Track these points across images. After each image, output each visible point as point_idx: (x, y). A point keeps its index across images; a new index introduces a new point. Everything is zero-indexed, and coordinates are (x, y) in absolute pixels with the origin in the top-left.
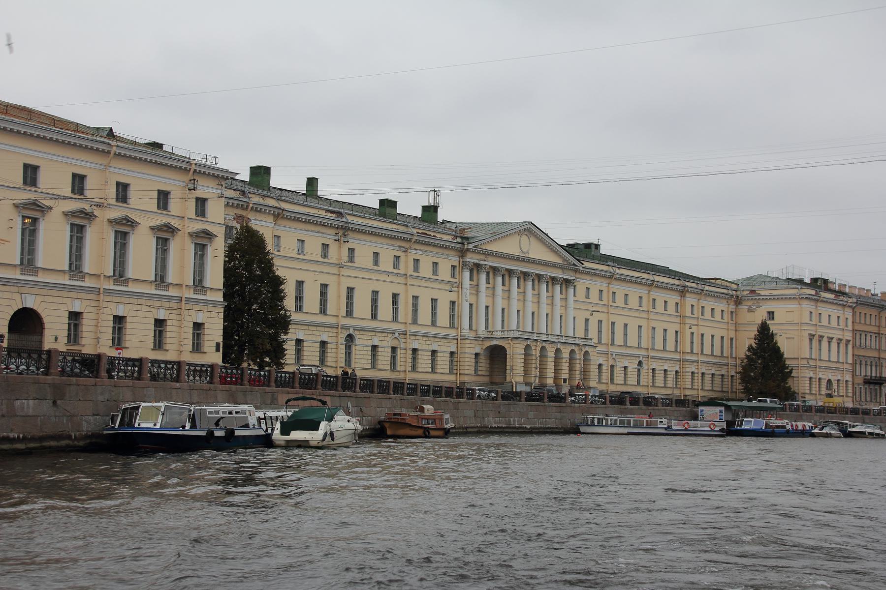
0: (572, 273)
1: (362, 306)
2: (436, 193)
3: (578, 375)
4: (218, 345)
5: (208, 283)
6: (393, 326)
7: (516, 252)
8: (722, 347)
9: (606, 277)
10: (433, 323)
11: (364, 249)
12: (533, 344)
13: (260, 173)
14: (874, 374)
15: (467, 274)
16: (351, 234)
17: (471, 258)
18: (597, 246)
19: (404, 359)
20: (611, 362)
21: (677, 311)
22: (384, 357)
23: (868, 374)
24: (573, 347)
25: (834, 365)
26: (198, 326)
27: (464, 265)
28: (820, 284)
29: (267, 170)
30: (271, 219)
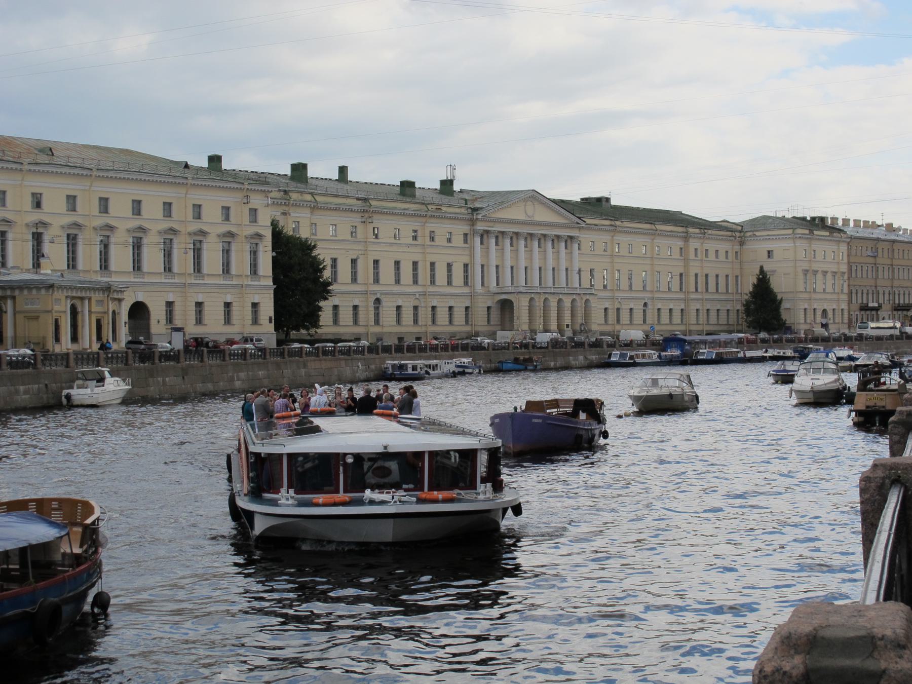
1: (387, 272)
2: (453, 168)
3: (580, 320)
4: (270, 318)
5: (261, 272)
6: (415, 289)
7: (522, 217)
8: (727, 285)
9: (609, 231)
10: (449, 283)
11: (386, 227)
12: (536, 297)
13: (299, 169)
14: (902, 302)
16: (375, 216)
17: (480, 227)
18: (608, 200)
19: (425, 315)
20: (617, 306)
21: (681, 255)
22: (407, 315)
23: (897, 302)
24: (574, 297)
25: (829, 297)
26: (255, 305)
28: (818, 223)
29: (304, 167)
30: (308, 211)
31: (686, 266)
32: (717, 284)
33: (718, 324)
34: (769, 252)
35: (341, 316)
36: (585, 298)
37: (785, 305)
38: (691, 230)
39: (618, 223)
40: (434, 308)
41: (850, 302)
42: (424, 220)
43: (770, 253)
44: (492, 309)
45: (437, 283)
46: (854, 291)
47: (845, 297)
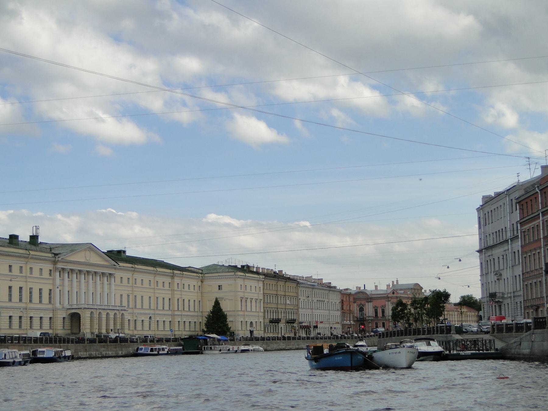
0: (114, 270)
2: (37, 228)
7: (83, 260)
9: (131, 271)
10: (40, 302)
12: (94, 311)
14: (274, 317)
15: (58, 274)
17: (60, 266)
18: (124, 252)
20: (135, 318)
21: (170, 287)
23: (272, 317)
27: (56, 269)
28: (246, 269)
31: (173, 294)
32: (163, 304)
33: (190, 331)
34: (219, 286)
35: (34, 323)
36: (121, 312)
37: (229, 319)
38: (176, 272)
39: (136, 266)
40: (31, 318)
41: (264, 318)
42: (26, 260)
43: (220, 287)
44: (66, 319)
45: (33, 302)
46: (266, 311)
47: (262, 314)
